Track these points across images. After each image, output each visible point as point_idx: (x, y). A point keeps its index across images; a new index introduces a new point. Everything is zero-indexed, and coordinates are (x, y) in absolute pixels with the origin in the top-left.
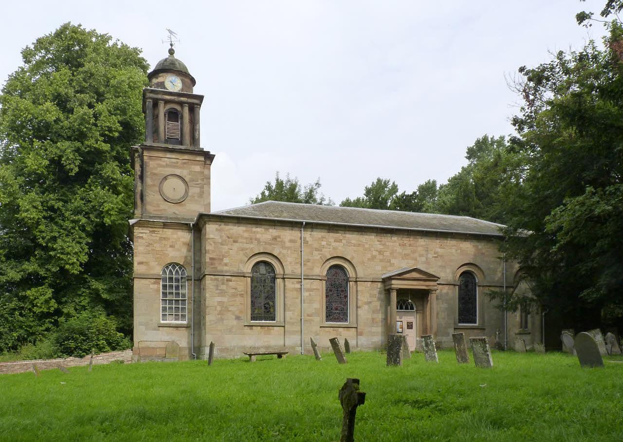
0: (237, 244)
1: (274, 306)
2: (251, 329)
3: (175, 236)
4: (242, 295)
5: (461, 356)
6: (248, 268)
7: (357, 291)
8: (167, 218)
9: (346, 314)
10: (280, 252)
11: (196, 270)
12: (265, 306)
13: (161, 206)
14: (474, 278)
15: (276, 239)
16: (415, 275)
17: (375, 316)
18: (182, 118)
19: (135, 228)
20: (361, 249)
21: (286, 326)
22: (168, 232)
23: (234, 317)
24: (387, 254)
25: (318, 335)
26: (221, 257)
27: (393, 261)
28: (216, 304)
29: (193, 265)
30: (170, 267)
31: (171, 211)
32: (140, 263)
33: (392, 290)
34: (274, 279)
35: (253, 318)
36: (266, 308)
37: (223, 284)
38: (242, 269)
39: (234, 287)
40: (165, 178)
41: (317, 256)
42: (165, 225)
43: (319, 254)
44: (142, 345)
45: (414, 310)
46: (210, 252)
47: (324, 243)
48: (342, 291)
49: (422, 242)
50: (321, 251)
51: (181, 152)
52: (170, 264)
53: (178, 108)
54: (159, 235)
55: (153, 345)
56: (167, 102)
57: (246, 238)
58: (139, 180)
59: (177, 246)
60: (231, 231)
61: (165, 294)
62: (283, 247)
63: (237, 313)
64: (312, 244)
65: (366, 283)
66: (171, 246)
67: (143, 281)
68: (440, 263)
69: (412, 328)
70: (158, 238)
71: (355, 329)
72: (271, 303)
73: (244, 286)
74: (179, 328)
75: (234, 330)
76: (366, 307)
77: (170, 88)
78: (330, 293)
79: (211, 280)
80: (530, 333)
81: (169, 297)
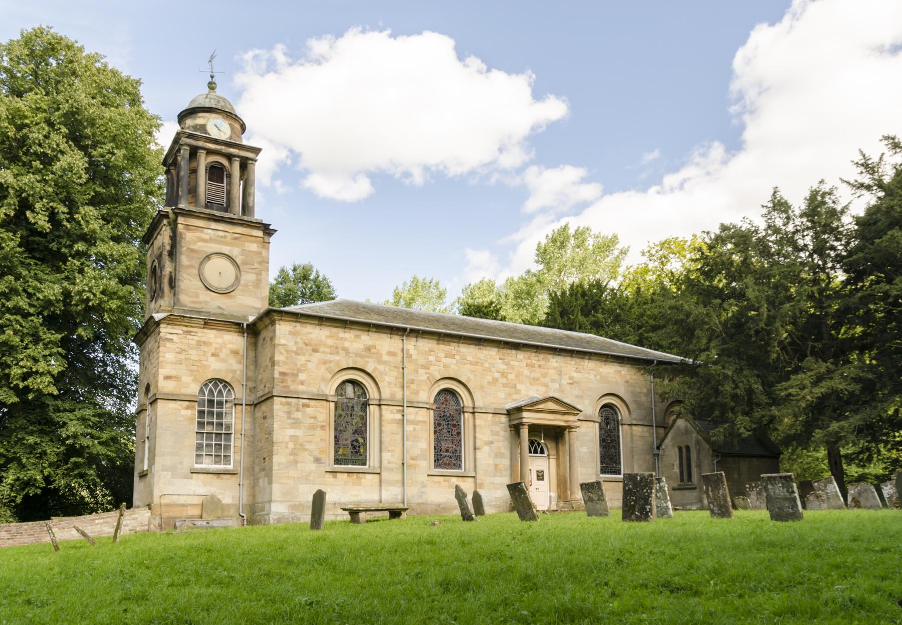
0: (317, 354)
1: (365, 444)
2: (335, 477)
3: (220, 341)
4: (322, 427)
5: (718, 505)
6: (330, 390)
7: (475, 426)
8: (209, 313)
9: (459, 458)
10: (375, 369)
11: (248, 391)
12: (352, 445)
13: (201, 296)
14: (616, 414)
15: (369, 350)
16: (551, 406)
17: (498, 461)
18: (229, 176)
19: (162, 326)
20: (479, 368)
21: (383, 474)
22: (210, 335)
23: (312, 459)
24: (512, 376)
25: (425, 486)
26: (295, 372)
27: (519, 387)
28: (287, 439)
29: (244, 383)
30: (210, 385)
31: (213, 304)
32: (167, 378)
33: (523, 425)
34: (365, 405)
35: (337, 461)
36: (354, 447)
37: (298, 410)
38: (324, 389)
39: (312, 415)
40: (208, 257)
41: (422, 375)
42: (207, 324)
43: (426, 373)
44: (165, 500)
45: (545, 455)
46: (281, 364)
47: (432, 358)
48: (454, 426)
49: (555, 362)
50: (429, 369)
51: (231, 222)
52: (211, 380)
53: (225, 162)
54: (196, 338)
55: (182, 500)
56: (210, 152)
57: (330, 347)
58: (167, 257)
59: (222, 355)
60: (311, 336)
61: (201, 424)
62: (380, 362)
63: (316, 453)
64: (417, 360)
65: (486, 415)
66: (213, 355)
67: (172, 405)
68: (576, 392)
69: (543, 479)
70: (194, 342)
71: (473, 479)
72: (361, 440)
73: (325, 413)
74: (222, 476)
75: (311, 478)
76: (486, 449)
77: (214, 133)
78: (439, 428)
79: (282, 404)
80: (695, 488)
81: (207, 429)
